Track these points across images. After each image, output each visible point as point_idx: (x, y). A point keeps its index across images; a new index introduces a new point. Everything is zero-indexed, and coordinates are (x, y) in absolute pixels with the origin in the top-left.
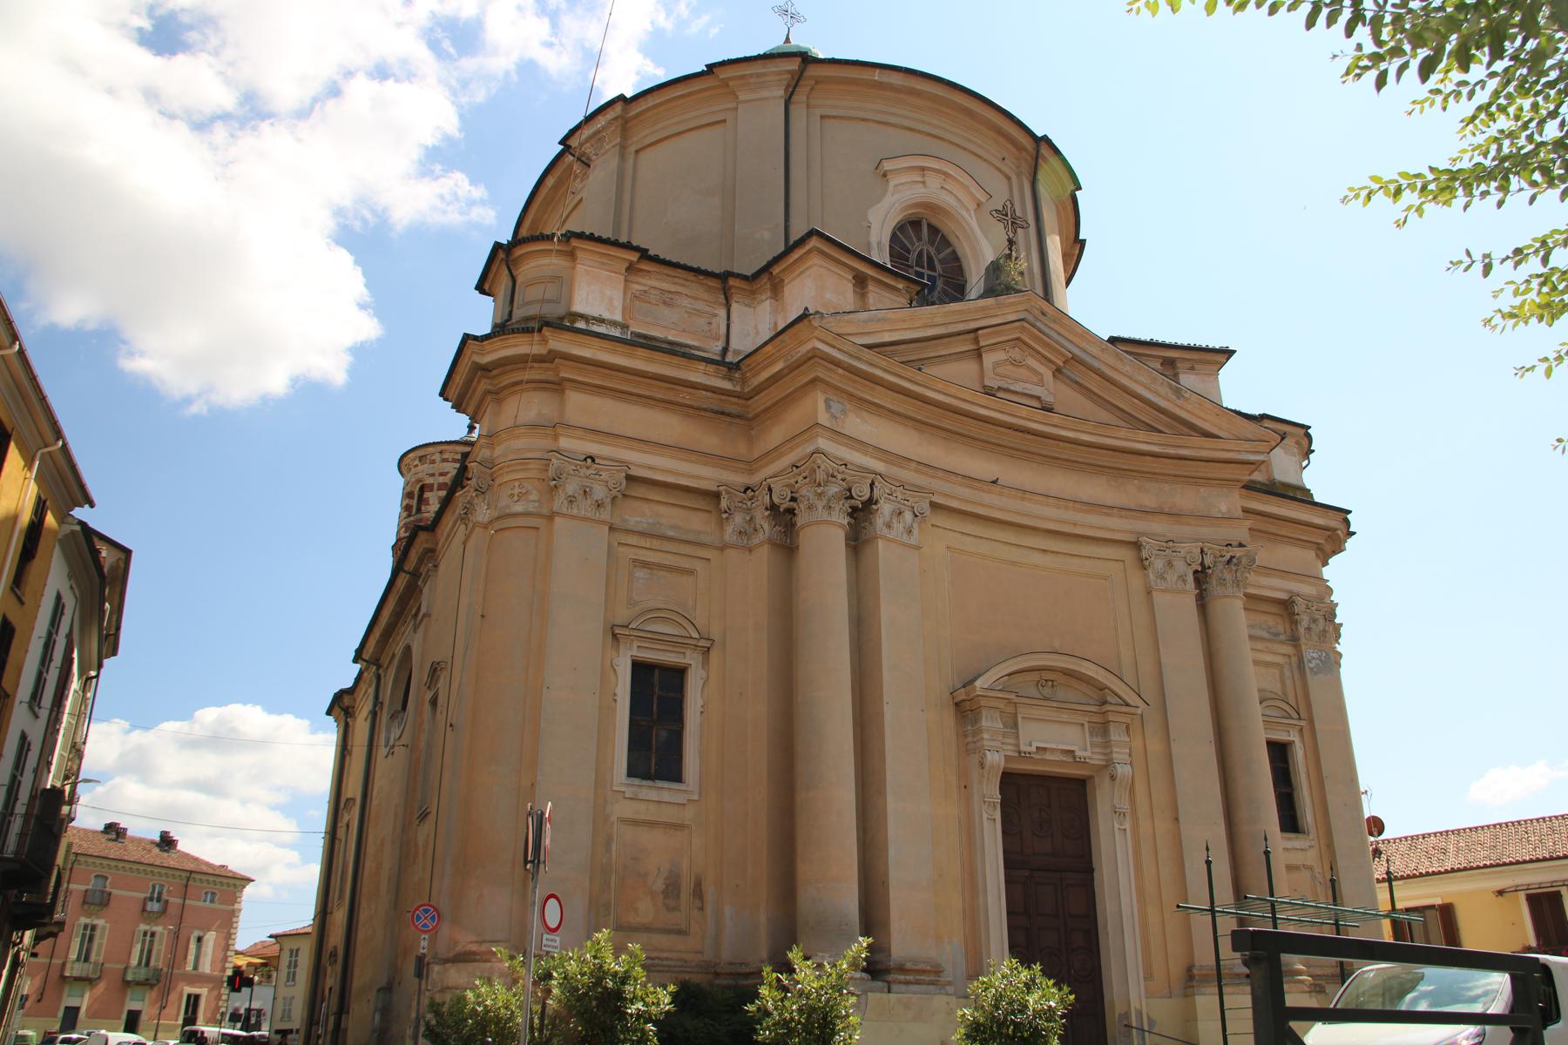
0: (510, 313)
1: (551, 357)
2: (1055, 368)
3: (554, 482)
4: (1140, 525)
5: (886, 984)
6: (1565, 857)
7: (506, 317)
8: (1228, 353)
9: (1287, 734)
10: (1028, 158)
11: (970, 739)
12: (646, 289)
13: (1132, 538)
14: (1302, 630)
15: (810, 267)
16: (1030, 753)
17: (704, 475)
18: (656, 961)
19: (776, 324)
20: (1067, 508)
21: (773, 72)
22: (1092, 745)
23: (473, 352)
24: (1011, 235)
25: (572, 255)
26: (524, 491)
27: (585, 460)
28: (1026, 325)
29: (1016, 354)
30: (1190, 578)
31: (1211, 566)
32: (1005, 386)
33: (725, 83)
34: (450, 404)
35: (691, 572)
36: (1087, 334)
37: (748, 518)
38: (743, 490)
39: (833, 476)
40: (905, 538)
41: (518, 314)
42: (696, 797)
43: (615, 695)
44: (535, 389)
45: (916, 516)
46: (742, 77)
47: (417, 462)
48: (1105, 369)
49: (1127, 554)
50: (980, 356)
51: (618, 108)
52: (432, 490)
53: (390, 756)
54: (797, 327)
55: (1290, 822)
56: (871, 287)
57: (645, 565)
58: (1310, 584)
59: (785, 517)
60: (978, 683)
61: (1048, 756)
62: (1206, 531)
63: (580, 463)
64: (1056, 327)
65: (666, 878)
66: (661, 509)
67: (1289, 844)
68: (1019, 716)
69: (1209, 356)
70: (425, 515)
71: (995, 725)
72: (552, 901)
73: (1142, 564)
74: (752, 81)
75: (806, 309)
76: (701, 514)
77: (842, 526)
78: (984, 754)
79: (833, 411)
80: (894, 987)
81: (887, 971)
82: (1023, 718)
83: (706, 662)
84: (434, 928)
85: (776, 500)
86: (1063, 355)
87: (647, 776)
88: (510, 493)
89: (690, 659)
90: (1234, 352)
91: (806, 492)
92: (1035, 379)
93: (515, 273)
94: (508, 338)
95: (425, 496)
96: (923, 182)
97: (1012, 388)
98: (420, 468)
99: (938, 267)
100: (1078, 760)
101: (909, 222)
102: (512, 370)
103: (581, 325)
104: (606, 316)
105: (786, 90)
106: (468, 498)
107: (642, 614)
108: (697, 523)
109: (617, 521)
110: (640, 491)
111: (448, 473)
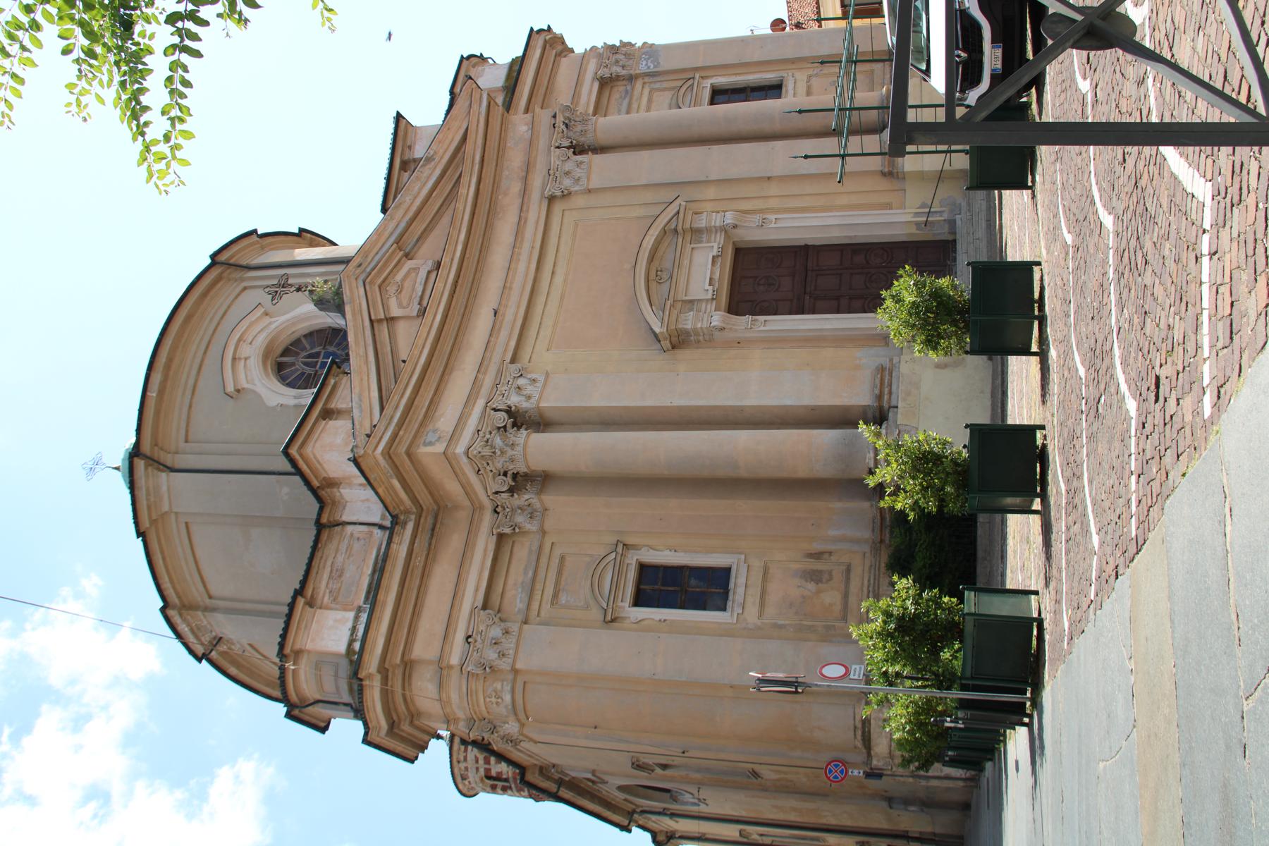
0: (346, 704)
1: (384, 671)
3: (487, 669)
4: (535, 195)
5: (891, 410)
7: (349, 708)
8: (399, 117)
10: (228, 271)
11: (701, 338)
12: (328, 591)
13: (545, 204)
14: (624, 72)
15: (315, 457)
17: (484, 545)
19: (361, 485)
22: (709, 241)
24: (293, 289)
25: (298, 653)
26: (494, 694)
27: (469, 643)
28: (368, 280)
29: (392, 289)
30: (579, 158)
32: (418, 299)
33: (153, 522)
34: (420, 755)
35: (562, 558)
36: (378, 232)
38: (496, 515)
39: (487, 441)
40: (539, 385)
41: (346, 698)
42: (743, 557)
43: (660, 621)
44: (410, 684)
46: (149, 508)
47: (466, 782)
48: (407, 218)
49: (558, 208)
50: (392, 319)
52: (490, 770)
53: (707, 802)
55: (773, 90)
56: (332, 405)
57: (556, 595)
61: (717, 276)
62: (542, 143)
65: (806, 581)
66: (511, 581)
67: (791, 92)
69: (401, 133)
70: (510, 775)
73: (566, 195)
74: (152, 499)
75: (349, 459)
76: (515, 550)
77: (528, 436)
78: (714, 327)
79: (433, 440)
80: (893, 403)
81: (881, 408)
84: (843, 765)
86: (393, 252)
88: (495, 705)
89: (632, 560)
93: (312, 701)
96: (246, 359)
97: (420, 294)
98: (471, 779)
99: (317, 349)
103: (357, 646)
104: (350, 624)
108: (522, 552)
109: (520, 618)
110: (495, 599)
111: (476, 757)
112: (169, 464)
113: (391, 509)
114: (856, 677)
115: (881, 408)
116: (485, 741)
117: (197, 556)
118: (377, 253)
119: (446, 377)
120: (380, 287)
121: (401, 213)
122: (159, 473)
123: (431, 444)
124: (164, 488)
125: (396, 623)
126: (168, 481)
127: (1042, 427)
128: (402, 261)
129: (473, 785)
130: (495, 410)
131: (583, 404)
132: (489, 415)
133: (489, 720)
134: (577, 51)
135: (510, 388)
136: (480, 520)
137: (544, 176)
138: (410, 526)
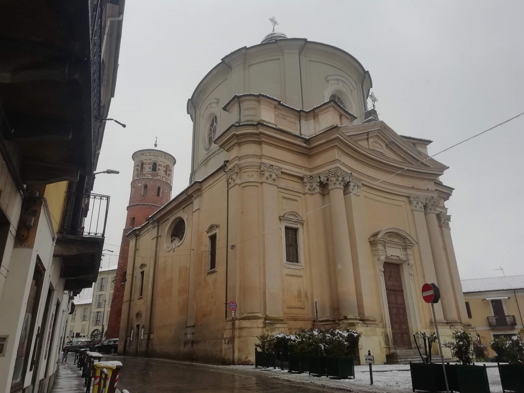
0: (240, 118)
6: (523, 289)
8: (430, 142)
11: (374, 252)
12: (278, 113)
14: (442, 223)
17: (301, 172)
25: (259, 102)
29: (376, 139)
35: (297, 201)
38: (309, 177)
41: (243, 119)
43: (281, 237)
47: (140, 155)
49: (405, 199)
56: (343, 118)
57: (285, 198)
59: (323, 186)
61: (393, 258)
68: (386, 246)
70: (144, 172)
73: (410, 202)
76: (298, 183)
78: (380, 257)
82: (387, 246)
89: (299, 226)
94: (246, 127)
95: (144, 166)
96: (338, 84)
97: (376, 150)
98: (142, 157)
101: (333, 96)
102: (242, 138)
103: (265, 124)
104: (270, 121)
108: (297, 186)
119: (303, 155)
122: (299, 50)
123: (338, 154)
127: (354, 378)
128: (385, 143)
129: (139, 158)
137: (415, 195)
138: (305, 145)
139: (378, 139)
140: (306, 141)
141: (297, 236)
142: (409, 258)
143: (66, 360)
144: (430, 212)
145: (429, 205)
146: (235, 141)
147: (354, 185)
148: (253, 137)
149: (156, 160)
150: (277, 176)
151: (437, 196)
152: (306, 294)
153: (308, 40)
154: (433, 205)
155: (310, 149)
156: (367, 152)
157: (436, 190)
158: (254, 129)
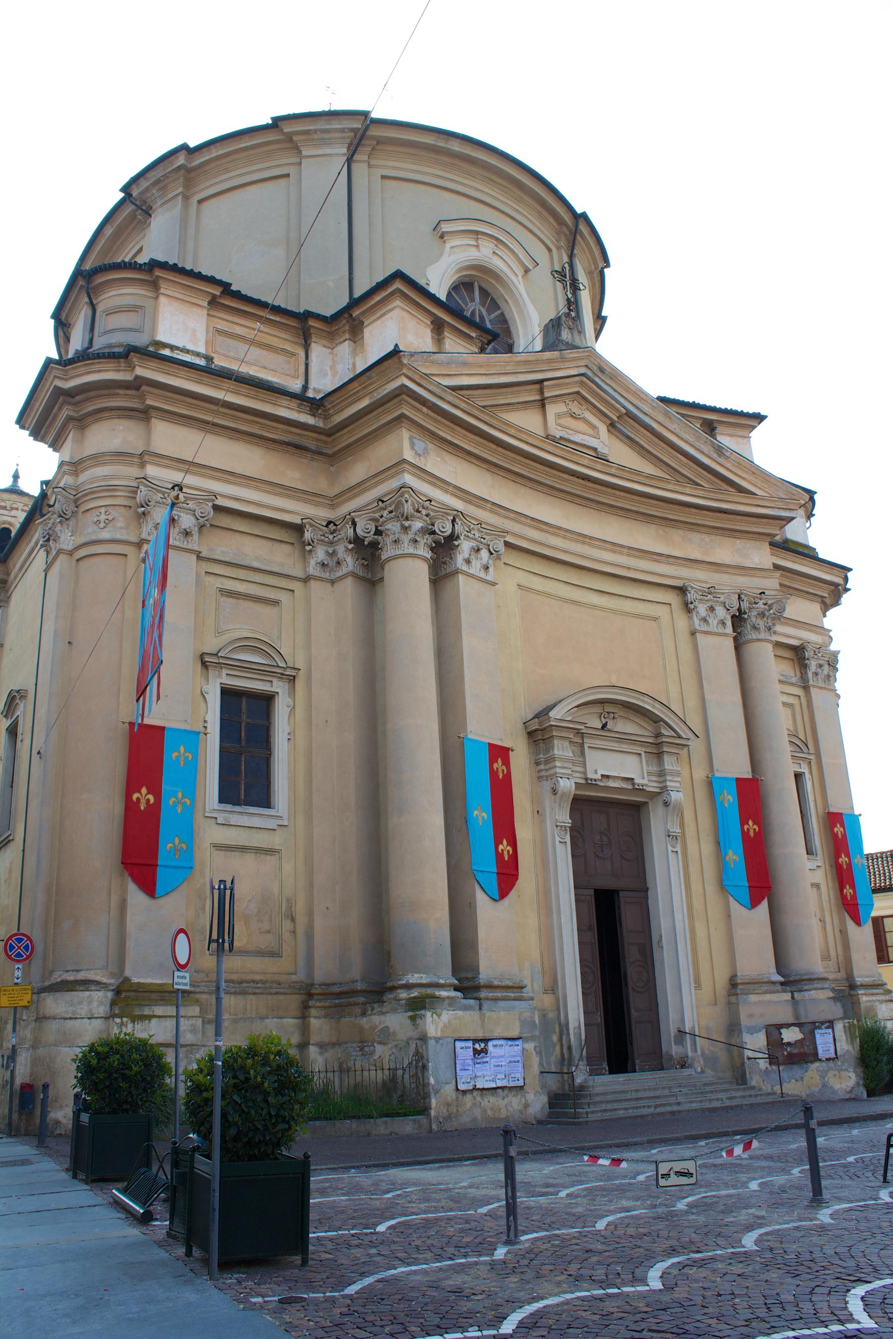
0: (91, 341)
1: (138, 384)
2: (609, 422)
3: (143, 509)
7: (86, 345)
8: (759, 418)
9: (798, 765)
10: (567, 233)
11: (542, 767)
13: (678, 583)
14: (810, 674)
15: (392, 309)
16: (595, 780)
18: (259, 985)
19: (354, 365)
20: (621, 553)
21: (336, 129)
22: (649, 773)
23: (55, 377)
25: (155, 285)
26: (110, 518)
27: (173, 488)
28: (585, 379)
29: (575, 408)
30: (729, 623)
31: (747, 611)
32: (566, 436)
33: (289, 138)
34: (27, 433)
35: (276, 603)
36: (639, 393)
37: (331, 551)
38: (325, 524)
41: (99, 343)
42: (285, 823)
43: (205, 722)
45: (491, 554)
46: (307, 132)
48: (655, 426)
50: (543, 406)
51: (181, 160)
54: (386, 364)
58: (817, 633)
60: (552, 714)
61: (611, 784)
63: (169, 491)
64: (612, 384)
66: (247, 540)
68: (586, 746)
69: (743, 421)
71: (566, 754)
72: (182, 936)
73: (688, 608)
74: (315, 136)
75: (396, 345)
77: (425, 559)
78: (557, 781)
80: (486, 1005)
81: (477, 988)
82: (589, 747)
83: (292, 691)
84: (28, 957)
85: (360, 532)
86: (617, 410)
87: (237, 802)
88: (95, 519)
89: (278, 687)
90: (765, 417)
91: (393, 527)
92: (591, 432)
94: (93, 363)
96: (477, 246)
97: (572, 438)
100: (637, 787)
103: (167, 352)
105: (348, 149)
106: (50, 525)
107: (231, 642)
110: (225, 521)
112: (357, 157)
113: (331, 399)
114: (176, 980)
115: (477, 988)
116: (45, 511)
117: (248, 188)
118: (615, 391)
120: (578, 393)
121: (656, 419)
124: (328, 151)
125: (195, 402)
126: (337, 155)
128: (605, 419)
130: (453, 521)
131: (464, 626)
132: (447, 514)
133: (76, 512)
134: (824, 619)
135: (475, 539)
136: (317, 505)
137: (706, 582)
138: (310, 420)
139: (584, 407)
140: (316, 405)
141: (272, 721)
142: (668, 784)
143: (482, 1040)
144: (754, 636)
145: (752, 617)
146: (66, 412)
147: (473, 548)
148: (118, 394)
149: (9, 519)
150: (198, 519)
151: (778, 587)
152: (290, 908)
153: (374, 115)
154: (762, 615)
155: (330, 433)
156: (527, 443)
157: (777, 567)
158: (119, 371)
